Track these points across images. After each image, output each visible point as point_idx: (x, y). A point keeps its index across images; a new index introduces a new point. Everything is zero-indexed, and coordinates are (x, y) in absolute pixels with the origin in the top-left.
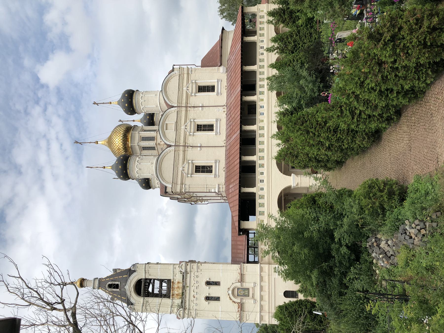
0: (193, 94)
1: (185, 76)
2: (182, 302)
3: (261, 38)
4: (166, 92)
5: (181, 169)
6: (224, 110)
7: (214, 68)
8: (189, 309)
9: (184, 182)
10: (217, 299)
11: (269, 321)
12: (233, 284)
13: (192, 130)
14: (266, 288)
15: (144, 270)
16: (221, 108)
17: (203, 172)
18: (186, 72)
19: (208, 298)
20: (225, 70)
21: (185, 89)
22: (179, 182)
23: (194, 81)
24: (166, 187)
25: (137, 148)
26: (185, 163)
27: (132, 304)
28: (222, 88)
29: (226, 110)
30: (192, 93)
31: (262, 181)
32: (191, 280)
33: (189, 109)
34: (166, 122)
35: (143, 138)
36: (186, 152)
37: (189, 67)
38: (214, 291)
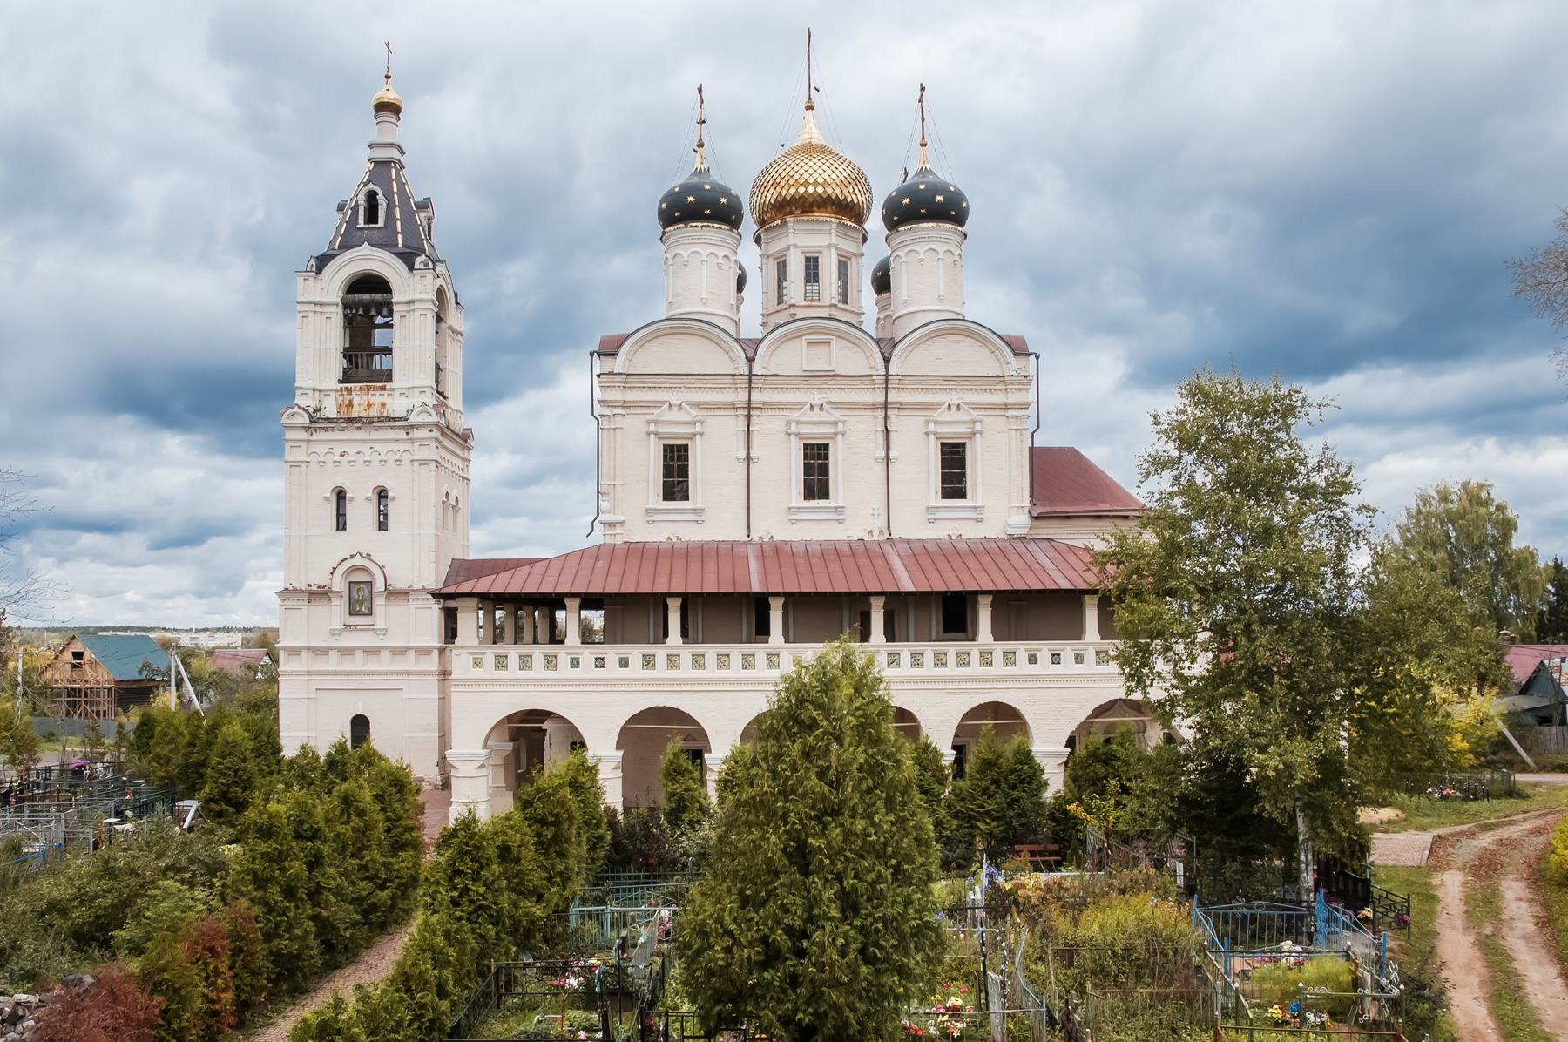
0: (932, 427)
1: (998, 398)
2: (328, 420)
3: (1090, 655)
4: (942, 333)
5: (675, 398)
6: (876, 532)
7: (1027, 493)
8: (308, 442)
9: (632, 411)
10: (341, 526)
11: (286, 673)
12: (382, 568)
13: (805, 430)
14: (373, 665)
15: (417, 297)
16: (882, 523)
17: (668, 471)
18: (1013, 397)
19: (341, 495)
20: (1017, 533)
21: (953, 398)
22: (631, 396)
23: (978, 427)
24: (613, 355)
26: (694, 412)
27: (319, 270)
28: (954, 524)
29: (876, 537)
30: (936, 423)
31: (600, 662)
32: (388, 443)
34: (834, 340)
35: (816, 259)
36: (731, 412)
37: (1032, 409)
38: (361, 512)
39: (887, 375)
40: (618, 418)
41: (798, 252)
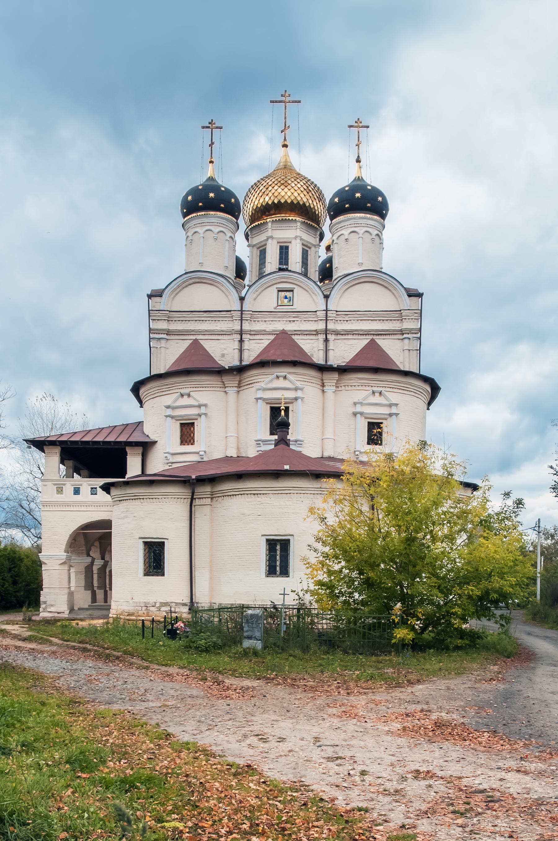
11: (50, 557)
22: (173, 326)
25: (262, 237)
31: (77, 491)
33: (322, 337)
35: (287, 248)
39: (242, 311)
40: (163, 342)
41: (275, 242)
